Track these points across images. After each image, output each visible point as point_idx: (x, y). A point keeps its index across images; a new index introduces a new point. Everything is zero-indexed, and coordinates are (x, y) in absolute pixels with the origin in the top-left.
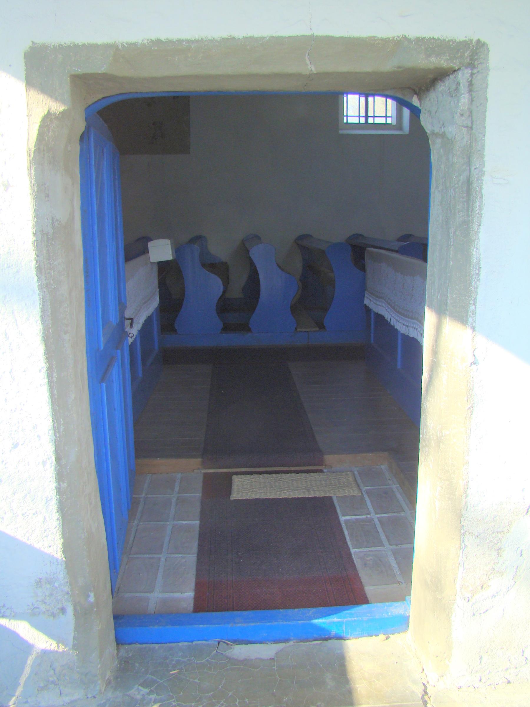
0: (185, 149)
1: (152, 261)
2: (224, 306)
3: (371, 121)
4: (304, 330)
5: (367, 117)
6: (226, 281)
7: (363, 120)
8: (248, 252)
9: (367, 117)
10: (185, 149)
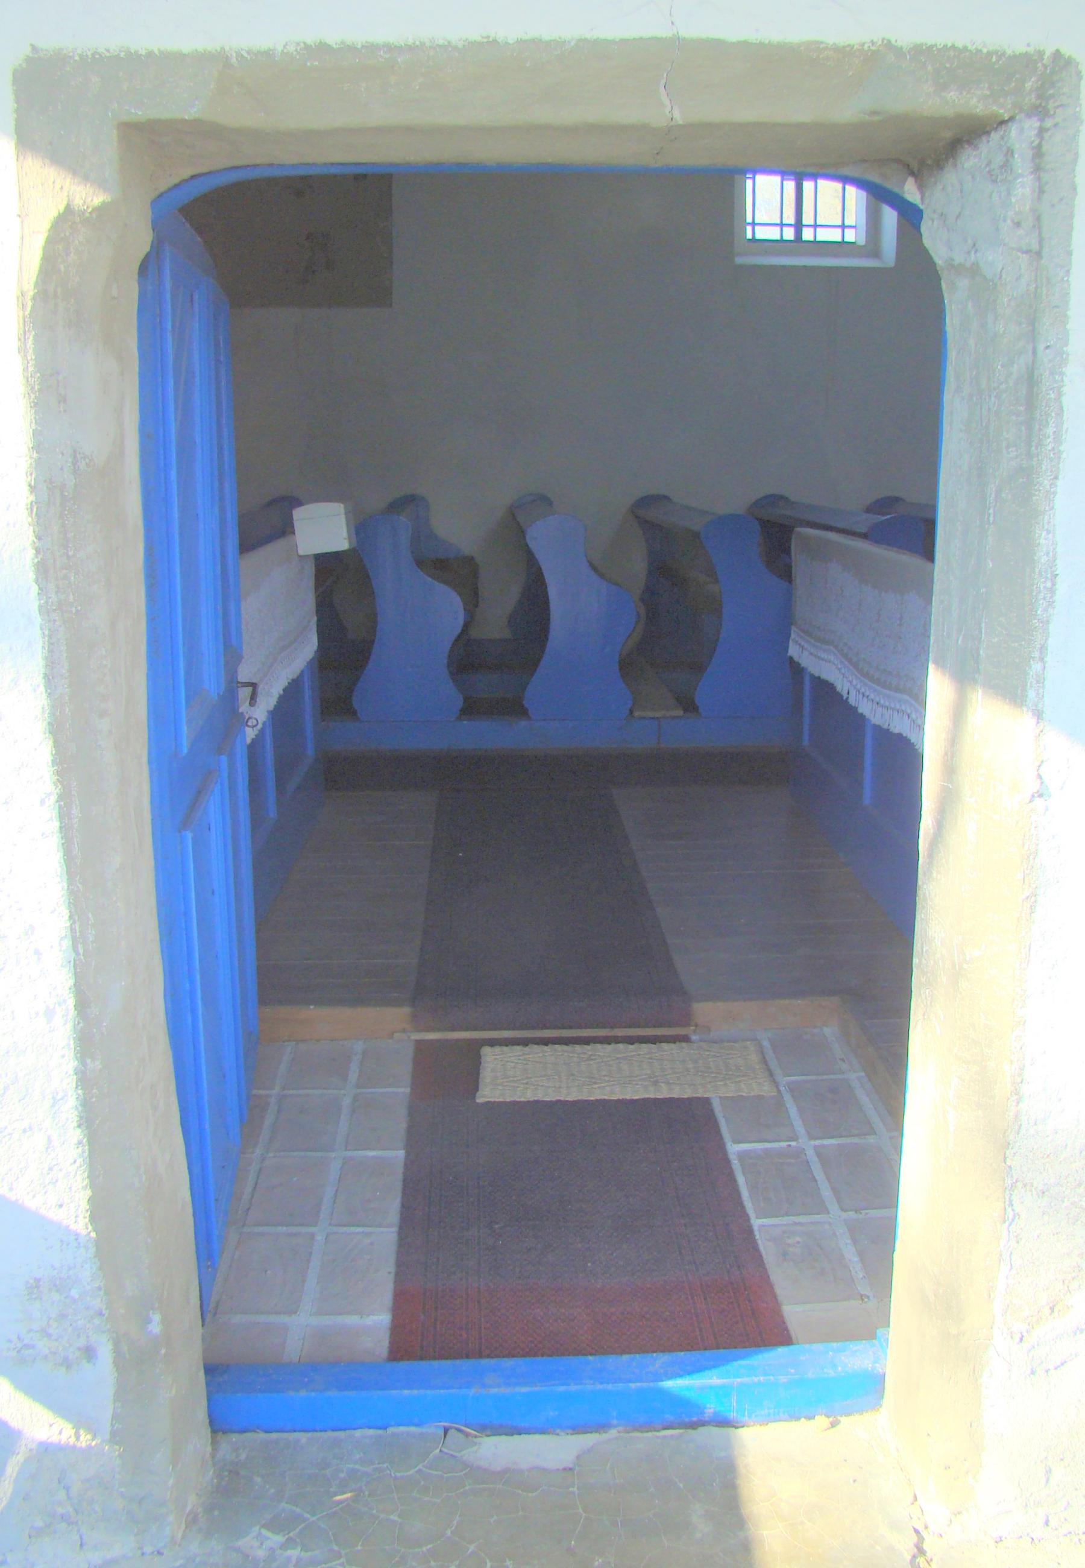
0: (380, 295)
1: (301, 552)
2: (467, 658)
3: (807, 235)
4: (650, 714)
5: (798, 226)
6: (472, 599)
7: (789, 234)
8: (523, 533)
9: (798, 226)
10: (380, 295)
